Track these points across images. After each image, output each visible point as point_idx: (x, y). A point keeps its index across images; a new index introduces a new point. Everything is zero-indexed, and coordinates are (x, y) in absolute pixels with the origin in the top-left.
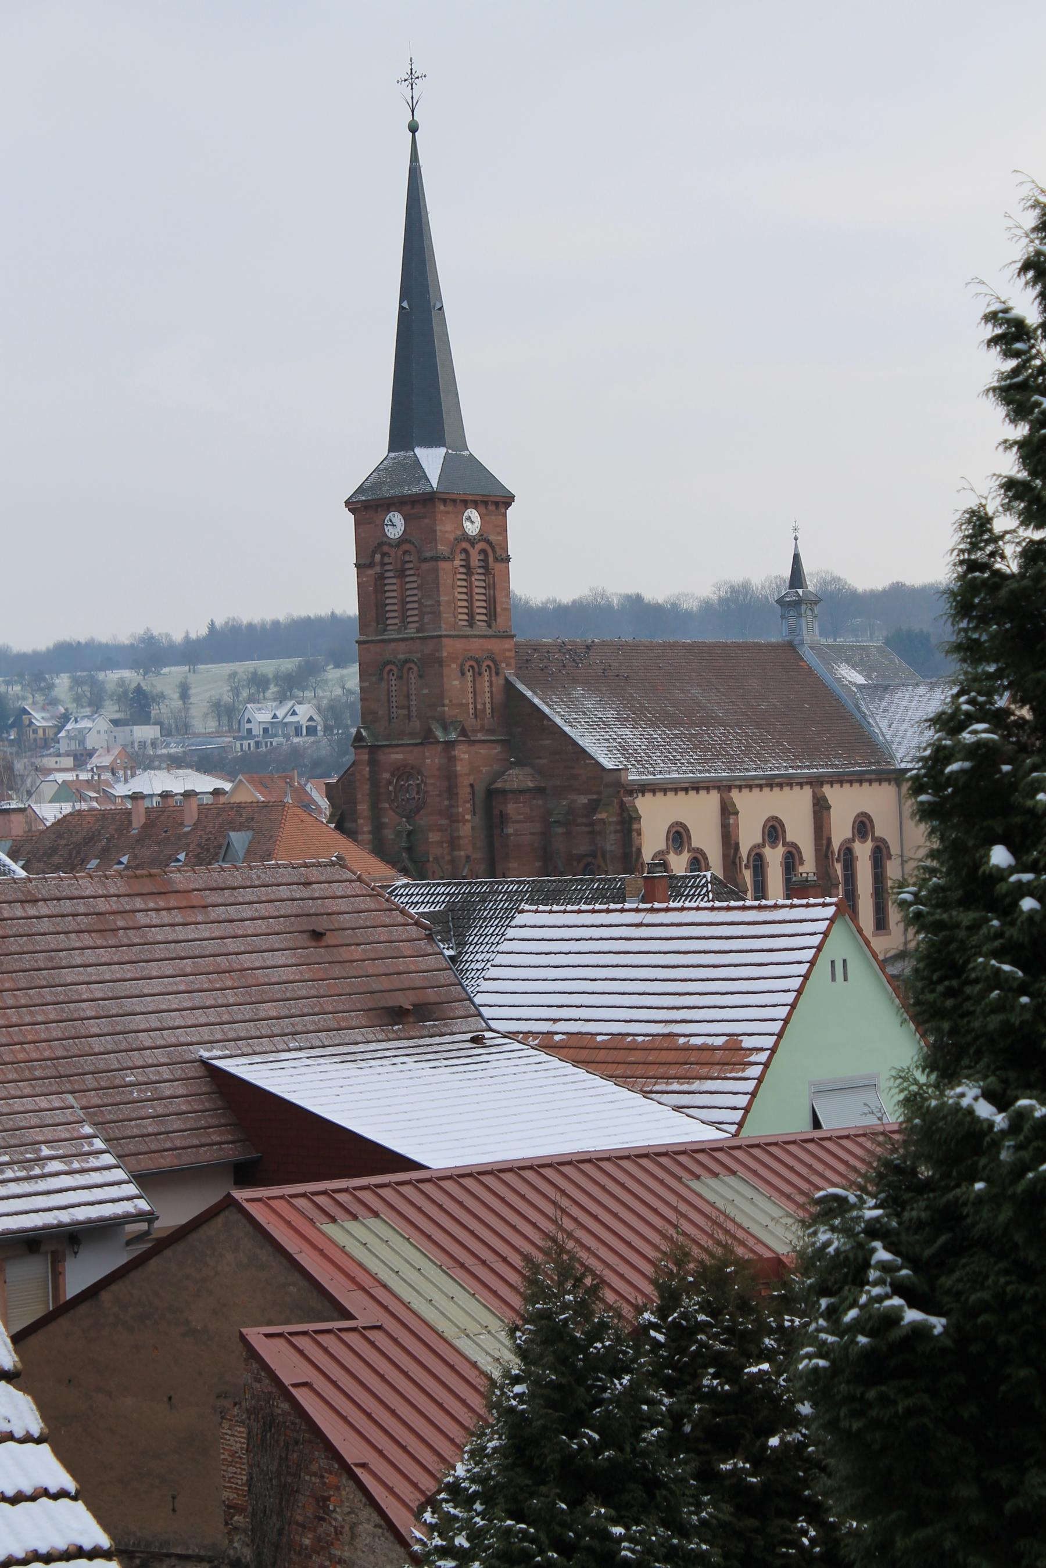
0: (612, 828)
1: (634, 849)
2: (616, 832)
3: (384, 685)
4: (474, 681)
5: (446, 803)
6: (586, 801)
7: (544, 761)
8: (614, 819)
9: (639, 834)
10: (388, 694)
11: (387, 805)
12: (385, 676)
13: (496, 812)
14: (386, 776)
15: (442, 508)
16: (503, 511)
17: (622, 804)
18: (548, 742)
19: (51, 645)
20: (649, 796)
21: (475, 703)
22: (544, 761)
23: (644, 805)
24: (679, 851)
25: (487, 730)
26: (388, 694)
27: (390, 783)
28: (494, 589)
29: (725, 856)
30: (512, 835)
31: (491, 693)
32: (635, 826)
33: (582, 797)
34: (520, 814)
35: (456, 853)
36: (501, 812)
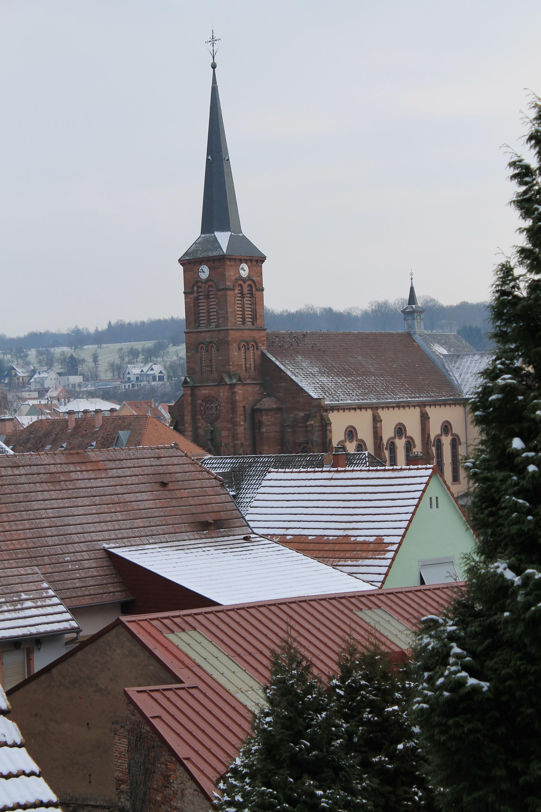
0: (317, 429)
1: (328, 440)
2: (319, 431)
3: (198, 355)
4: (245, 353)
5: (231, 416)
6: (303, 415)
7: (281, 394)
8: (318, 424)
9: (331, 432)
10: (201, 359)
11: (200, 417)
12: (199, 350)
13: (257, 420)
14: (200, 402)
15: (229, 263)
16: (260, 264)
17: (322, 416)
18: (283, 384)
19: (26, 334)
20: (335, 412)
21: (246, 364)
22: (281, 394)
23: (333, 417)
24: (351, 441)
25: (252, 378)
26: (201, 359)
27: (202, 405)
28: (256, 305)
29: (375, 444)
30: (265, 432)
31: (254, 359)
32: (328, 428)
33: (301, 413)
34: (269, 422)
35: (236, 442)
36: (259, 420)
